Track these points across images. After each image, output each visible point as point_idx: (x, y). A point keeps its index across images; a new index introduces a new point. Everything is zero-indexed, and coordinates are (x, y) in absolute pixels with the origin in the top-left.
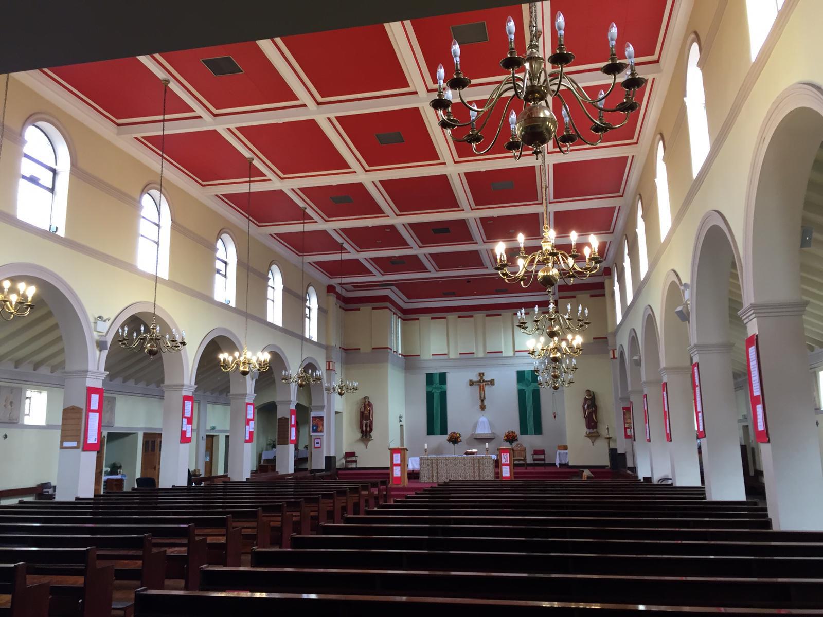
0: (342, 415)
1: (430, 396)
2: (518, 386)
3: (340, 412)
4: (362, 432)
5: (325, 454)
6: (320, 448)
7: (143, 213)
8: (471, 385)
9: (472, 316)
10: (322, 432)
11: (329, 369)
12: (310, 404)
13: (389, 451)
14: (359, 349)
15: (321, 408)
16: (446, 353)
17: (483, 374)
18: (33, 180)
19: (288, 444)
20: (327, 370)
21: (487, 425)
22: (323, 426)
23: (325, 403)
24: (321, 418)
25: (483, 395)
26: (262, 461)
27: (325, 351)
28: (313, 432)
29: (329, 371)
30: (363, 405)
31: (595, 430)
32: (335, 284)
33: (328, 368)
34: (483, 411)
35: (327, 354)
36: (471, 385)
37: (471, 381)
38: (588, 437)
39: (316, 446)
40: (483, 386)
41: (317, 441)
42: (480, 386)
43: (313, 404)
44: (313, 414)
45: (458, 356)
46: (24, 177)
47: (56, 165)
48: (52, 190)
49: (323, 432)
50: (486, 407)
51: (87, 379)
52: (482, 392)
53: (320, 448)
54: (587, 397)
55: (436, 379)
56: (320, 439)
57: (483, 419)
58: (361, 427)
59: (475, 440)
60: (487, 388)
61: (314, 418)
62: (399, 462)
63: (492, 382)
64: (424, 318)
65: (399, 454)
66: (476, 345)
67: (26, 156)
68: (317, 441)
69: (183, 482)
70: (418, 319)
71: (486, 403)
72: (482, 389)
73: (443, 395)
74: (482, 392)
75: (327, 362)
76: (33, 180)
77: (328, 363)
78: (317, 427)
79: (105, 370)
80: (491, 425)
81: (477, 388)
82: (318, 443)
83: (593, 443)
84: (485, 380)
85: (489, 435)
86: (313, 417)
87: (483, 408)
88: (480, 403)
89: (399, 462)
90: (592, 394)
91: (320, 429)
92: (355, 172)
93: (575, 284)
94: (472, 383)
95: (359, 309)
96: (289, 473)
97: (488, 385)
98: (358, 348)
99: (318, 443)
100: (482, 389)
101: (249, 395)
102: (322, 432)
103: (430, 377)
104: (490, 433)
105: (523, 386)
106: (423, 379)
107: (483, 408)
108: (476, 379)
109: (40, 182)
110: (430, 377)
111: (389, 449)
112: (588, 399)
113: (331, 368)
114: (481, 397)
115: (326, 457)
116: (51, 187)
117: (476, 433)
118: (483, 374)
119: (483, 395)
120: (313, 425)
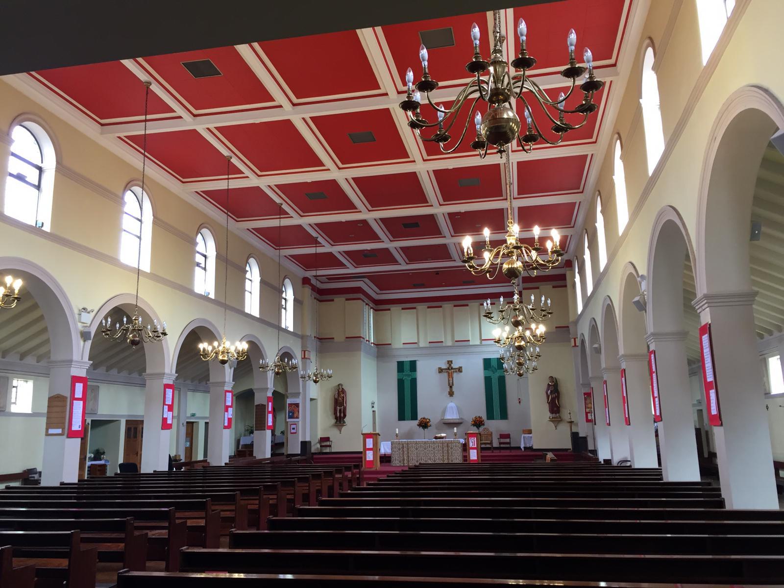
1: (401, 383)
2: (485, 374)
4: (336, 418)
5: (301, 439)
7: (13, 148)
8: (439, 372)
9: (441, 307)
10: (297, 418)
12: (287, 391)
14: (333, 338)
15: (297, 395)
16: (416, 342)
17: (451, 361)
18: (20, 177)
19: (265, 430)
20: (302, 358)
22: (298, 412)
24: (297, 405)
27: (300, 340)
31: (558, 415)
33: (303, 357)
36: (439, 372)
37: (440, 368)
38: (552, 421)
41: (293, 426)
43: (289, 391)
44: (289, 401)
45: (428, 345)
46: (11, 175)
47: (42, 163)
48: (38, 187)
52: (451, 379)
54: (550, 384)
55: (407, 367)
56: (296, 424)
60: (455, 375)
62: (371, 446)
63: (460, 370)
64: (395, 309)
65: (372, 439)
67: (13, 154)
68: (293, 426)
69: (164, 467)
70: (389, 310)
71: (454, 389)
72: (450, 376)
73: (414, 382)
74: (451, 379)
76: (20, 177)
77: (303, 352)
78: (293, 414)
80: (459, 410)
82: (294, 429)
83: (556, 427)
85: (457, 420)
86: (289, 404)
87: (451, 394)
88: (448, 389)
90: (554, 380)
91: (295, 416)
94: (441, 370)
95: (333, 300)
96: (198, 460)
99: (294, 429)
100: (450, 376)
102: (297, 418)
103: (401, 365)
104: (458, 418)
105: (489, 373)
106: (394, 367)
107: (451, 394)
108: (444, 366)
110: (401, 365)
112: (551, 385)
117: (445, 418)
118: (451, 361)
119: (451, 381)
120: (289, 411)
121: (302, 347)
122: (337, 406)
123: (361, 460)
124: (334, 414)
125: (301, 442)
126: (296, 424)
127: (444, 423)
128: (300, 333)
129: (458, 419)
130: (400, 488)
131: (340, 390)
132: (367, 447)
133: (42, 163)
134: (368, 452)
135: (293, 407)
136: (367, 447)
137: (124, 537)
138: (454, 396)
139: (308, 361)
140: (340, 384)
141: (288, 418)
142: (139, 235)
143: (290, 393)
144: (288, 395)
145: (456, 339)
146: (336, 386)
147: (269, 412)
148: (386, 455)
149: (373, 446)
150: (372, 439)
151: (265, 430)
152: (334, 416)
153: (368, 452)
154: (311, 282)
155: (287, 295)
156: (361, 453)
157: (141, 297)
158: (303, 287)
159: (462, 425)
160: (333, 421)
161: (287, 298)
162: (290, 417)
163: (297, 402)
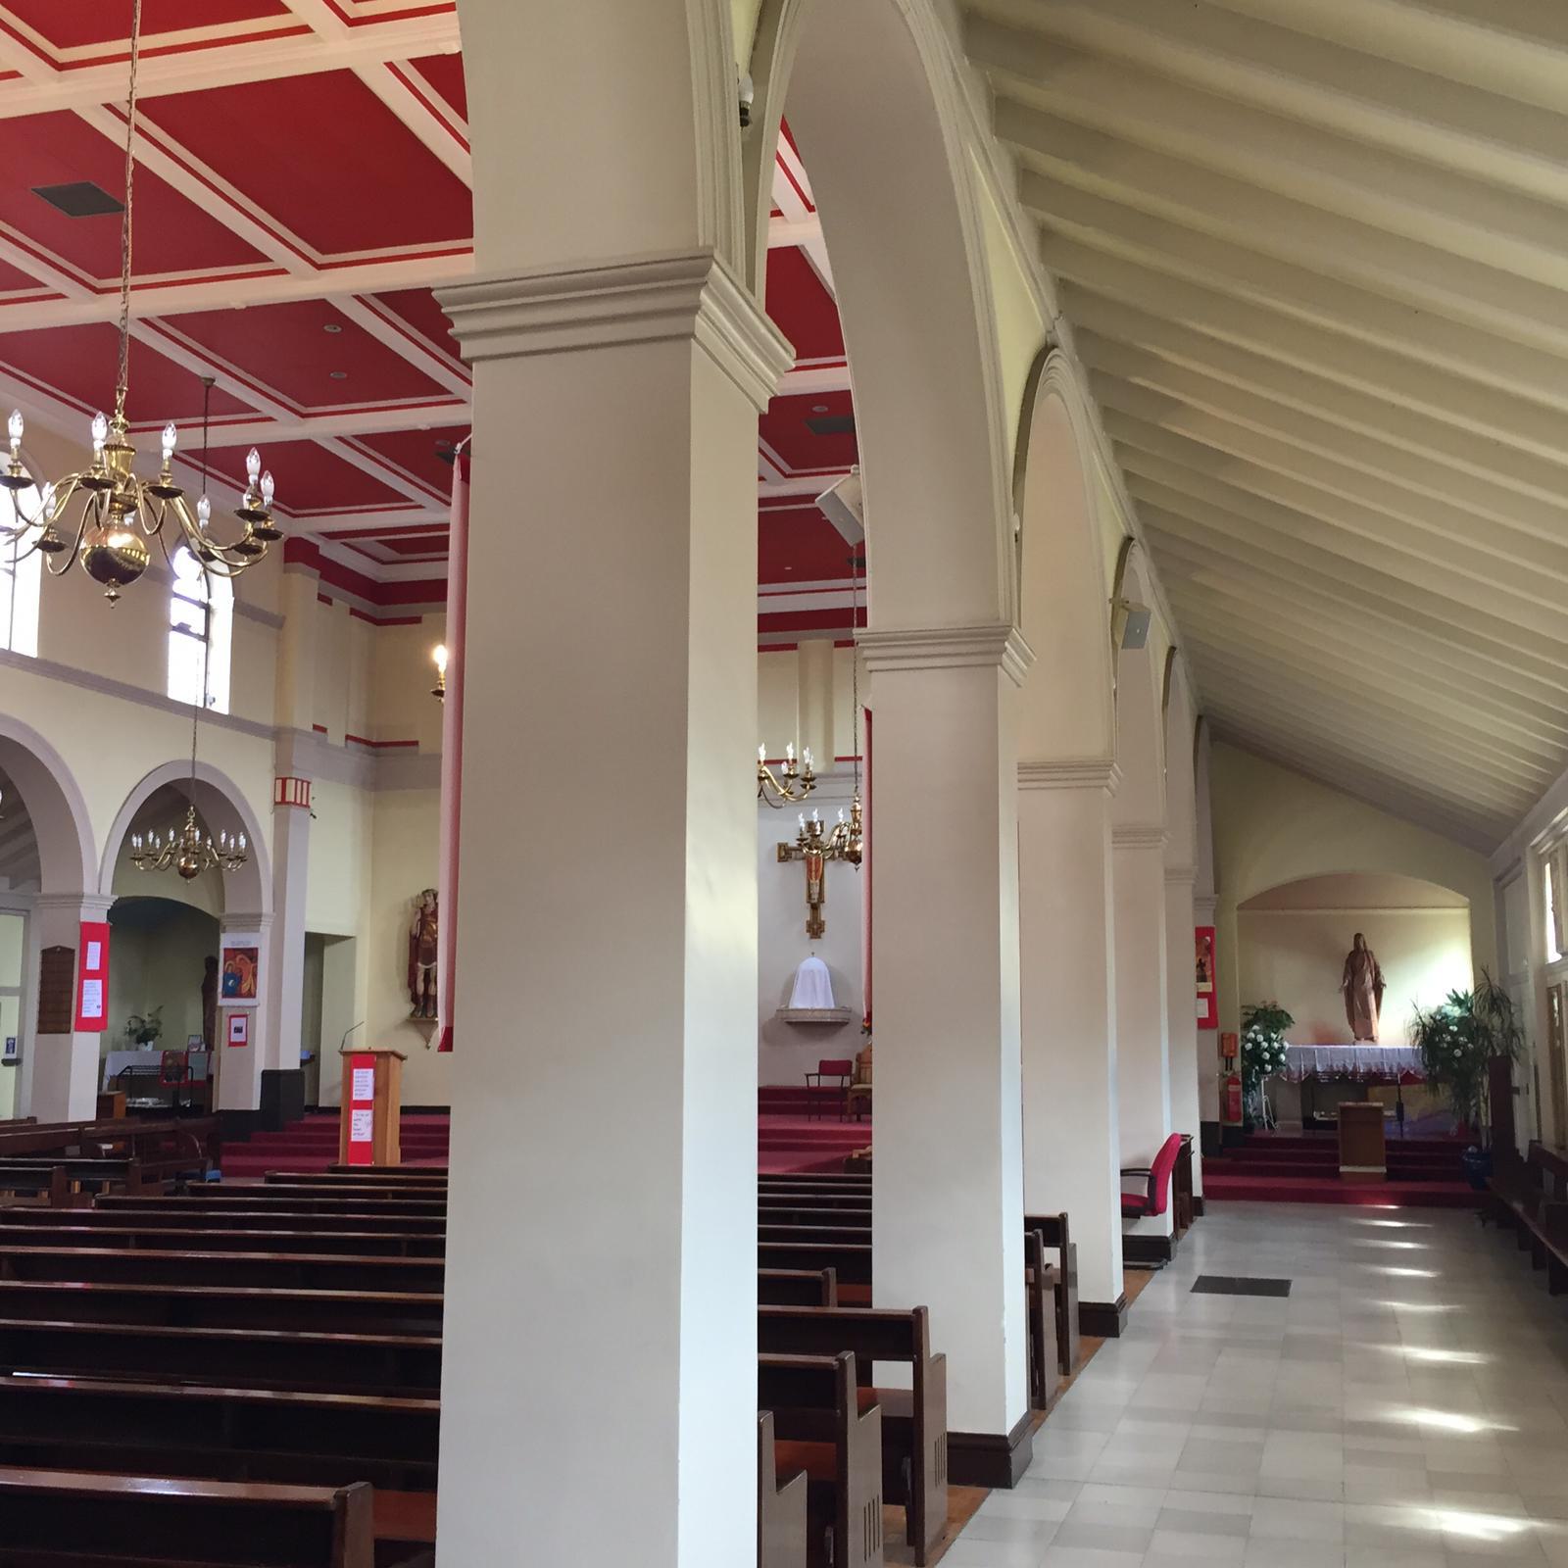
0: (354, 947)
3: (350, 937)
4: (415, 998)
5: (261, 1064)
6: (244, 1044)
7: (177, 587)
8: (781, 859)
9: (793, 647)
10: (251, 994)
11: (284, 801)
12: (222, 908)
13: (342, 1057)
14: (415, 743)
15: (252, 921)
18: (183, 629)
19: (69, 1032)
20: (276, 803)
21: (823, 982)
22: (255, 975)
23: (267, 906)
24: (251, 954)
25: (816, 889)
26: (106, 1082)
27: (268, 745)
28: (226, 995)
29: (283, 808)
30: (419, 916)
32: (311, 533)
33: (279, 799)
34: (816, 941)
35: (278, 755)
36: (781, 859)
37: (782, 847)
39: (236, 1037)
40: (817, 863)
41: (236, 1022)
42: (809, 864)
43: (228, 910)
44: (227, 941)
46: (174, 629)
47: (209, 597)
48: (206, 638)
49: (254, 997)
50: (827, 927)
51: (82, 909)
52: (815, 882)
53: (244, 1044)
56: (245, 1016)
57: (814, 965)
58: (412, 983)
59: (790, 1031)
60: (830, 869)
61: (231, 953)
62: (368, 1095)
65: (371, 1071)
66: (802, 728)
67: (176, 595)
68: (236, 1022)
72: (815, 872)
74: (815, 882)
75: (277, 779)
76: (183, 629)
77: (279, 782)
78: (239, 980)
79: (112, 893)
80: (836, 981)
81: (801, 865)
82: (238, 1030)
84: (226, 566)
85: (829, 1014)
86: (225, 950)
87: (815, 929)
88: (807, 915)
89: (368, 1095)
91: (245, 987)
92: (305, 29)
93: (986, 1486)
95: (417, 620)
96: (70, 1120)
97: (832, 858)
98: (413, 739)
99: (238, 1030)
100: (815, 872)
101: (92, 897)
102: (251, 994)
104: (833, 1007)
107: (815, 929)
109: (191, 630)
111: (345, 1054)
113: (290, 797)
114: (810, 896)
115: (266, 1074)
116: (202, 633)
117: (790, 1007)
119: (816, 889)
120: (225, 973)
121: (276, 767)
122: (417, 961)
123: (406, 1135)
124: (410, 986)
125: (266, 1074)
126: (245, 1016)
127: (790, 1023)
128: (267, 719)
129: (832, 1010)
130: (814, 1187)
131: (430, 909)
132: (355, 1098)
133: (209, 597)
134: (355, 1113)
135: (238, 959)
136: (355, 1098)
137: (1230, 1086)
138: (823, 935)
139: (294, 811)
140: (427, 891)
141: (224, 996)
142: (13, 543)
143: (229, 916)
144: (224, 922)
145: (838, 753)
146: (418, 896)
147: (93, 975)
148: (838, 1118)
149: (376, 1092)
150: (371, 1071)
151: (69, 1032)
152: (408, 993)
153: (355, 1113)
154: (321, 552)
155: (213, 594)
156: (336, 1111)
157: (201, 760)
158: (285, 571)
159: (846, 1028)
160: (408, 1008)
161: (212, 602)
162: (230, 993)
163: (252, 945)
